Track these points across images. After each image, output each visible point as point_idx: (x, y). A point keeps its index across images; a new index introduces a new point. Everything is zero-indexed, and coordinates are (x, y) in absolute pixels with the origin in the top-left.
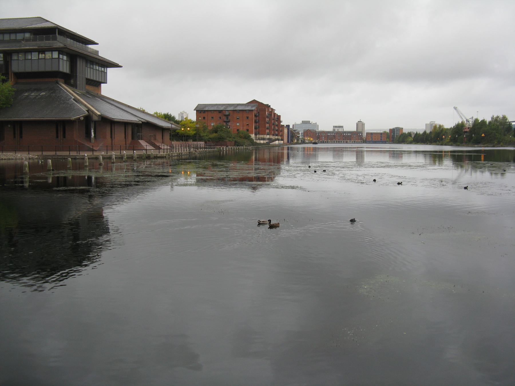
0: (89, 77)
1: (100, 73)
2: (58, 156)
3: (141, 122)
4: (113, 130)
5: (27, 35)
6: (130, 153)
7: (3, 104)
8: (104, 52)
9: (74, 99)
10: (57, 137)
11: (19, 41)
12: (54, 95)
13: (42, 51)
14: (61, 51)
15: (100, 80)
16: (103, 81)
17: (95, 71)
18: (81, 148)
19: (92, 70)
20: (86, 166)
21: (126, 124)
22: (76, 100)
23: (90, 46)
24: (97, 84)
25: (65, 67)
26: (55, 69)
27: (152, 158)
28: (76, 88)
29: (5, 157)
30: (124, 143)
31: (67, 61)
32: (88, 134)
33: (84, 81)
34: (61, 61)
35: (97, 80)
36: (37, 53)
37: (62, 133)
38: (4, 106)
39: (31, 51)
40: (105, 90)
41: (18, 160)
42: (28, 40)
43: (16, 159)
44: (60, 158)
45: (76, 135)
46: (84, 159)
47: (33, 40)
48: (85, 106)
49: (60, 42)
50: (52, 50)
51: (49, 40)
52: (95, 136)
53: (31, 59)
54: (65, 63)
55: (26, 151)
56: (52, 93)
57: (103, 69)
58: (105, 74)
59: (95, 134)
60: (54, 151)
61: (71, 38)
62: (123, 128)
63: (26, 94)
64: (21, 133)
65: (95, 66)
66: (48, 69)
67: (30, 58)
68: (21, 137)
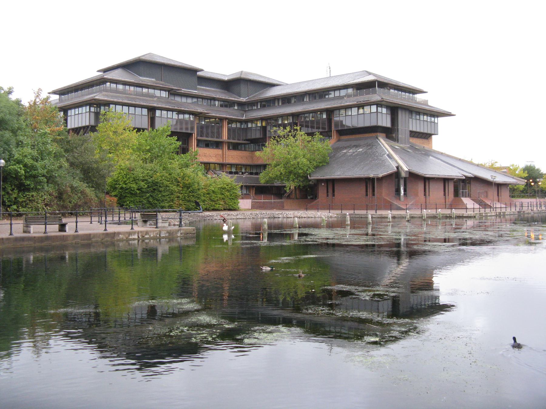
0: (414, 130)
1: (429, 124)
2: (355, 214)
3: (464, 178)
4: (427, 187)
5: (350, 91)
6: (447, 212)
7: (320, 163)
8: (432, 99)
9: (388, 155)
10: (367, 195)
11: (342, 98)
12: (370, 151)
13: (360, 106)
14: (379, 104)
15: (429, 132)
16: (433, 133)
17: (422, 122)
18: (390, 207)
19: (418, 121)
20: (347, 225)
21: (445, 181)
22: (390, 156)
23: (419, 97)
24: (427, 136)
25: (385, 121)
26: (374, 124)
27: (453, 218)
28: (398, 142)
29: (305, 216)
30: (444, 201)
31: (387, 114)
32: (398, 191)
33: (408, 134)
34: (379, 115)
35: (426, 131)
36: (375, 106)
37: (371, 191)
38: (321, 165)
39: (350, 107)
40: (437, 143)
41: (317, 219)
42: (349, 96)
43: (315, 217)
44: (357, 217)
45: (385, 192)
46: (367, 218)
47: (355, 96)
48: (396, 162)
49: (378, 95)
50: (370, 104)
51: (369, 94)
52: (405, 194)
53: (351, 115)
54: (384, 116)
55: (327, 209)
56: (369, 149)
57: (433, 119)
58: (436, 124)
59: (405, 190)
60: (352, 209)
61: (395, 89)
62: (365, 184)
63: (345, 151)
64: (333, 191)
65: (422, 117)
66: (367, 124)
67: (350, 114)
68: (334, 195)
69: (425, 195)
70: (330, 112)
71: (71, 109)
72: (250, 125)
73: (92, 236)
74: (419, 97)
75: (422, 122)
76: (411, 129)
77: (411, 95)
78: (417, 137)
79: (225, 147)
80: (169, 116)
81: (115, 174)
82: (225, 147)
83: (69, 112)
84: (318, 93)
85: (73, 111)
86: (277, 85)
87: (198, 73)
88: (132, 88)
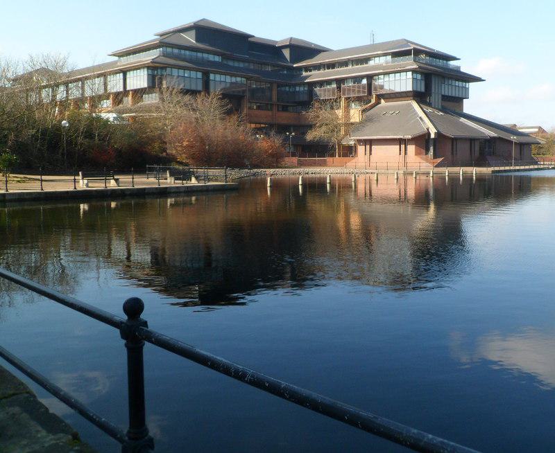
40: (468, 107)
58: (467, 90)
69: (452, 153)
70: (370, 78)
71: (130, 71)
72: (297, 89)
73: (168, 190)
74: (452, 63)
75: (454, 87)
76: (443, 93)
77: (445, 62)
78: (449, 101)
79: (275, 108)
80: (222, 80)
81: (83, 123)
82: (275, 108)
83: (128, 73)
84: (479, 139)
85: (132, 72)
86: (324, 51)
87: (249, 39)
88: (187, 52)
